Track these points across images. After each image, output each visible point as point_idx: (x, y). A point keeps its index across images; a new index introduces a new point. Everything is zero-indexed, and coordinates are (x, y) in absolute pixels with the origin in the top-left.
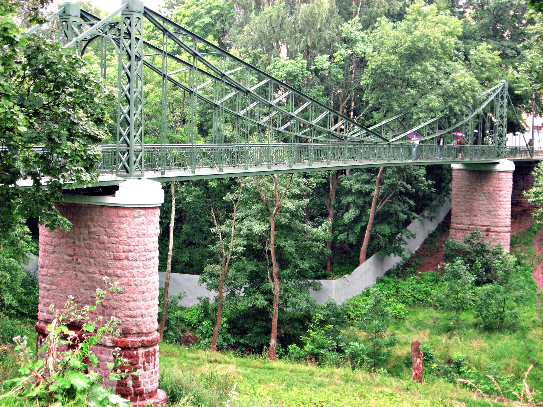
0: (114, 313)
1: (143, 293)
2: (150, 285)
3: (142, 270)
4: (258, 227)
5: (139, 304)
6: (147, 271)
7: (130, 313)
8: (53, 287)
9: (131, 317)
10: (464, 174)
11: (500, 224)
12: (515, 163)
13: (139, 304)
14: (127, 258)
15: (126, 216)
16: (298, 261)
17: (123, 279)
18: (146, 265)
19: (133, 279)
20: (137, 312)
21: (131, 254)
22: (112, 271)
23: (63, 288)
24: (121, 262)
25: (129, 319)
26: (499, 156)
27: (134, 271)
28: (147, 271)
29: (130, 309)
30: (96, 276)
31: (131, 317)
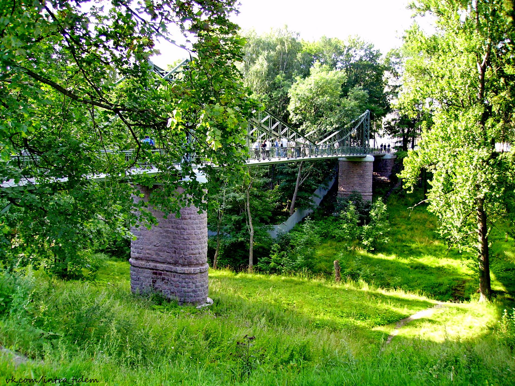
0: (182, 253)
1: (200, 239)
2: (204, 234)
3: (198, 225)
4: (241, 197)
5: (197, 246)
6: (201, 226)
7: (192, 252)
8: (141, 237)
9: (193, 254)
10: (346, 163)
11: (367, 191)
12: (374, 156)
13: (197, 246)
14: (190, 218)
15: (467, 9)
16: (203, 198)
17: (187, 231)
18: (201, 222)
19: (194, 231)
20: (197, 251)
21: (192, 216)
22: (180, 226)
23: (148, 237)
24: (186, 221)
25: (191, 256)
26: (365, 153)
27: (195, 226)
28: (201, 226)
29: (192, 250)
30: (169, 229)
31: (193, 254)
